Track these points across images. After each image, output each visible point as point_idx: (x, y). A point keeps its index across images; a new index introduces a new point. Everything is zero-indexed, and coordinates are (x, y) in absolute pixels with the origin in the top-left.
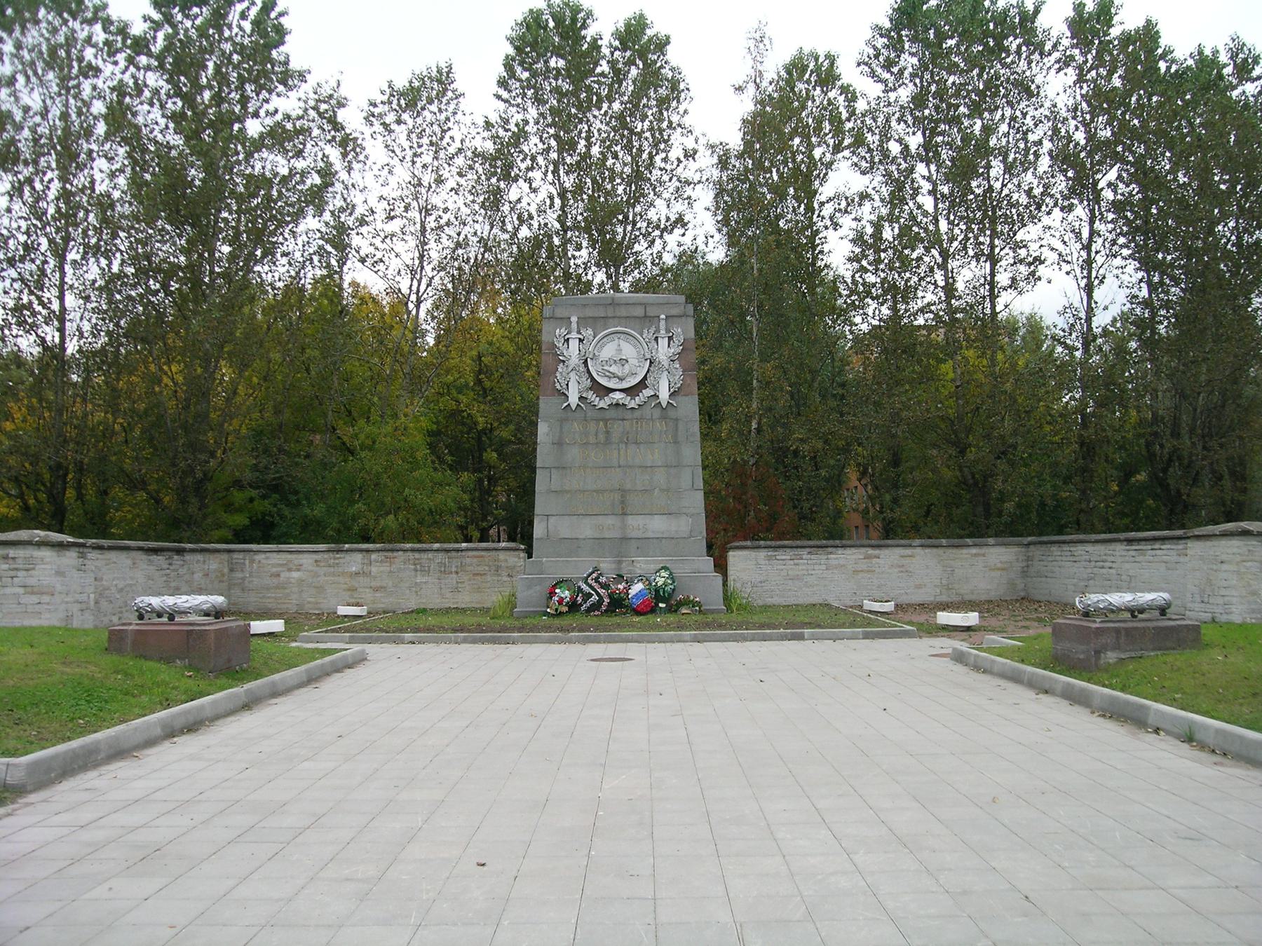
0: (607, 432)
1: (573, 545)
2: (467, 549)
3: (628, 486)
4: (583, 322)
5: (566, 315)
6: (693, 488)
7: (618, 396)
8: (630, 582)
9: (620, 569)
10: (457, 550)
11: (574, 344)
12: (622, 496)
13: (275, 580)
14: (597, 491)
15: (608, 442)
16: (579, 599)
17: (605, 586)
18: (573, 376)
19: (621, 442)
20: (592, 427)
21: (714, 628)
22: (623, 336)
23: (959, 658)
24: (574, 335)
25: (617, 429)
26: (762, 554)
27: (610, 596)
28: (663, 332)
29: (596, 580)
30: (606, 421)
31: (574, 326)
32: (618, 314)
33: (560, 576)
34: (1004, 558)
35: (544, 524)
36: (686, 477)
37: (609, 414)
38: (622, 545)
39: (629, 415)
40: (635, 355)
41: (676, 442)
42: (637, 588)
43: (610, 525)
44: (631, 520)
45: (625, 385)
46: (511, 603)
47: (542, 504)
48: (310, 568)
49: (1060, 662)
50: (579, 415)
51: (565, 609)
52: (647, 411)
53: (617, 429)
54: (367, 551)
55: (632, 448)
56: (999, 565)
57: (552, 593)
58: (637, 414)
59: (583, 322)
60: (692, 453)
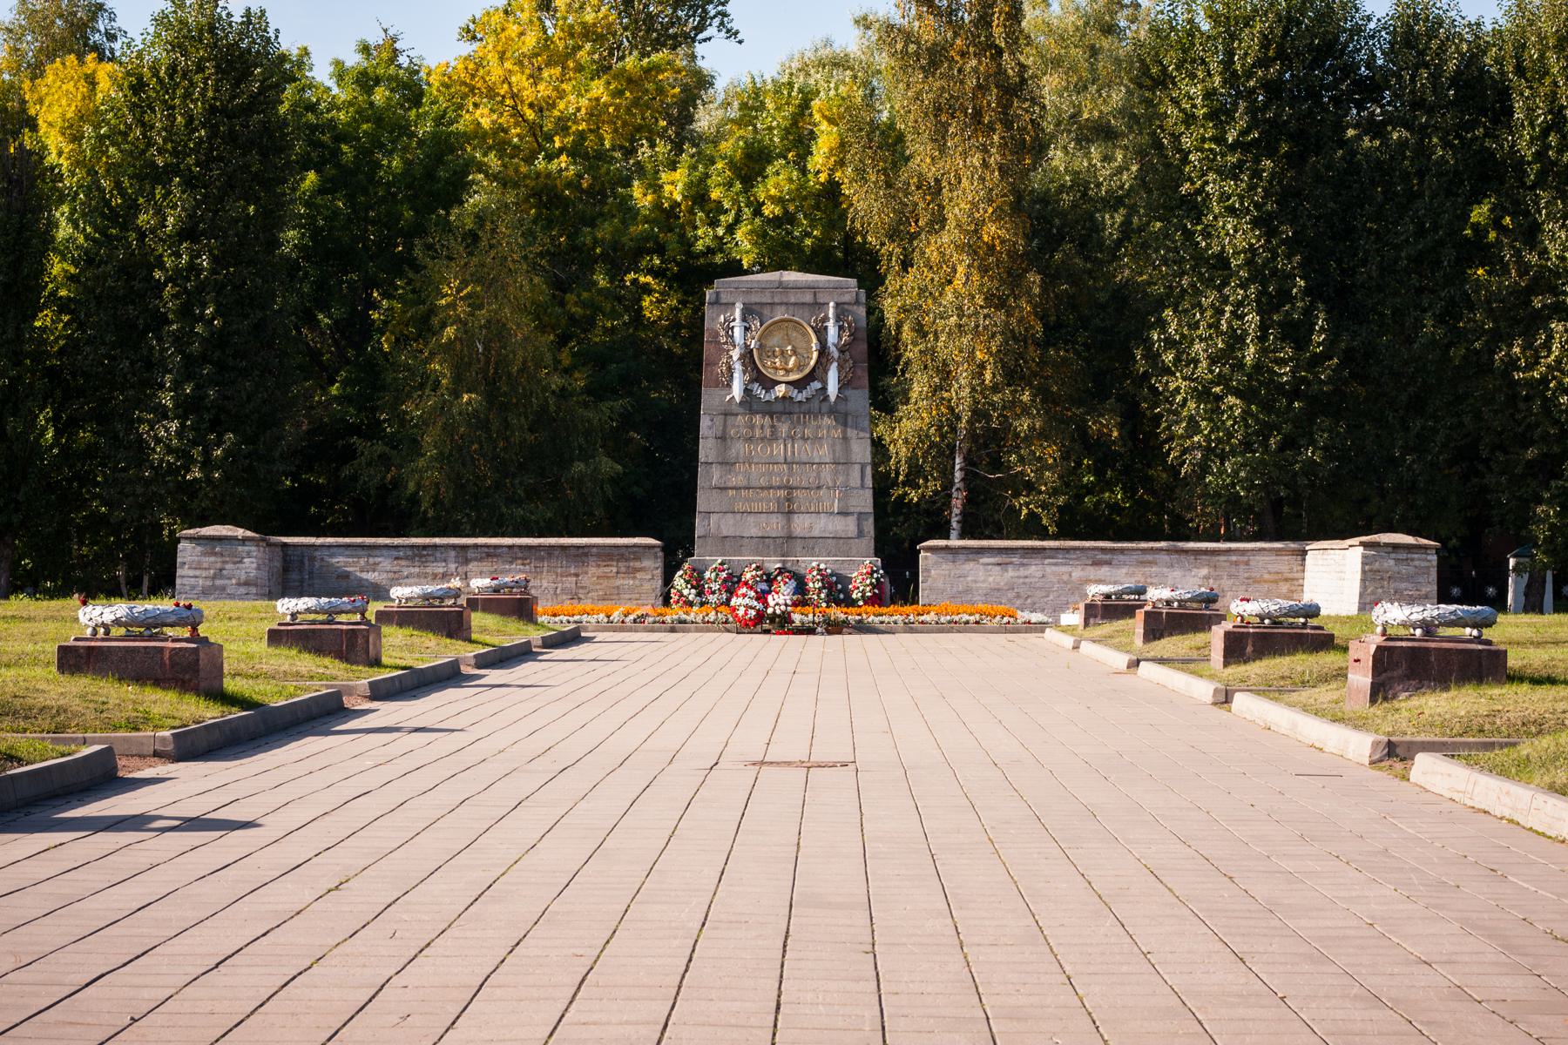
43: (775, 525)
52: (815, 404)
58: (804, 408)
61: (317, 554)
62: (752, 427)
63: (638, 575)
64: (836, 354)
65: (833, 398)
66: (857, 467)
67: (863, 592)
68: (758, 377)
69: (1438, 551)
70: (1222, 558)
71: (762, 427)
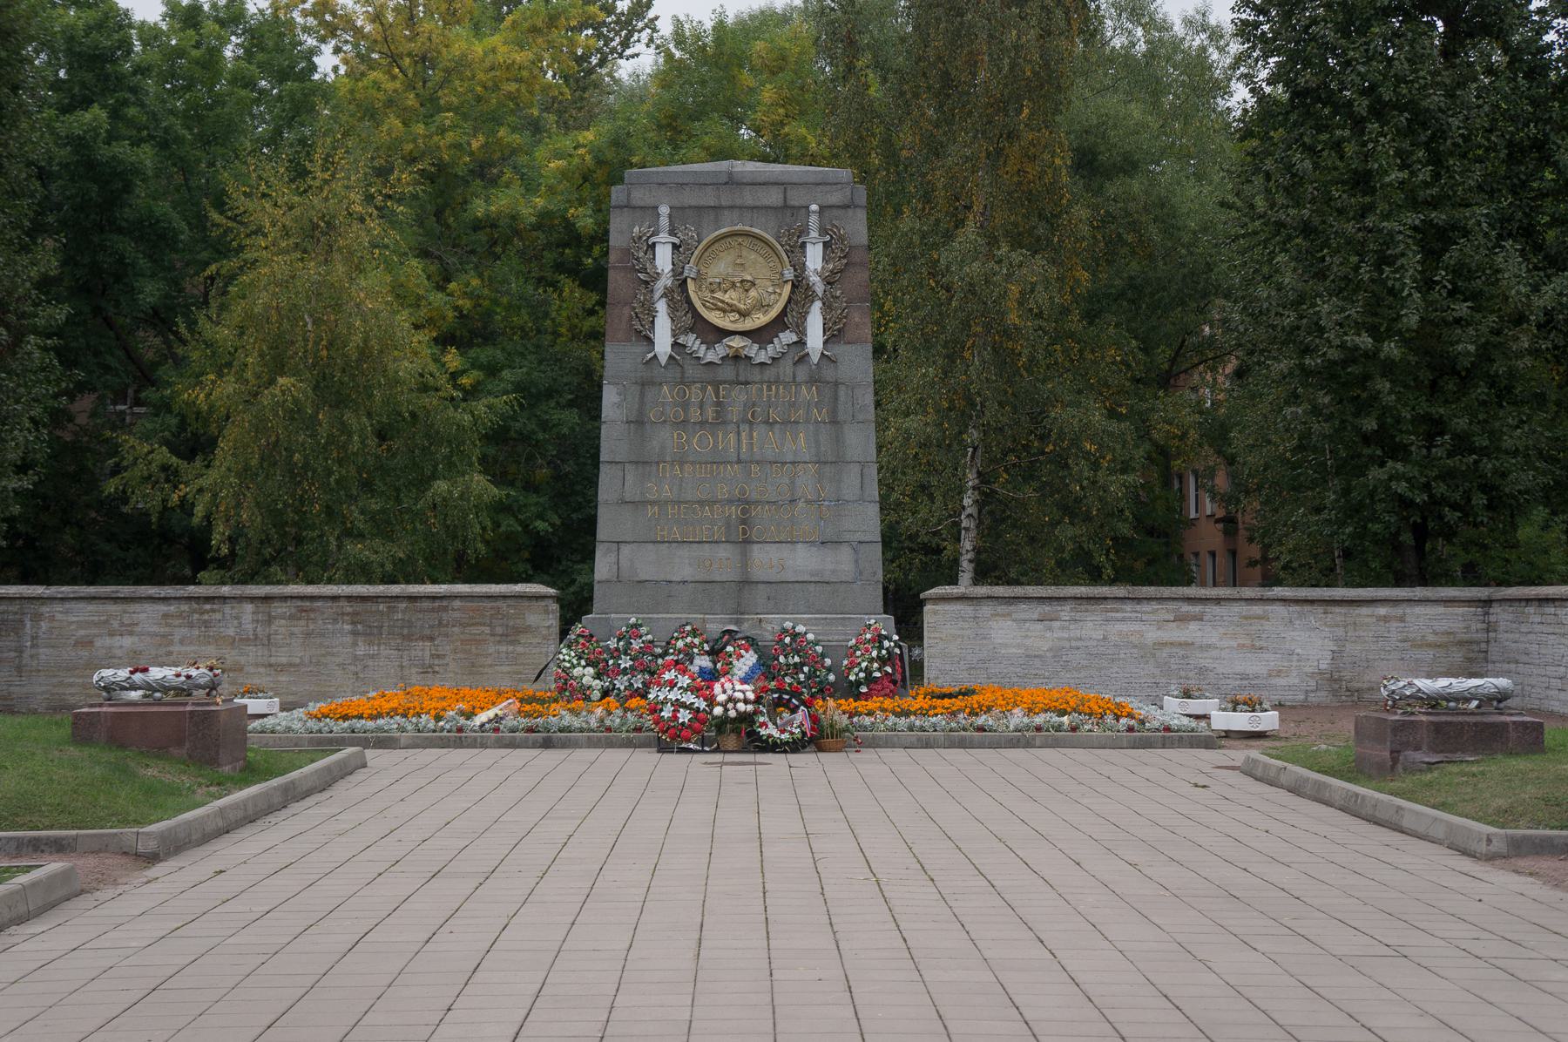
1: (660, 592)
5: (649, 201)
6: (861, 499)
12: (744, 512)
13: (85, 653)
14: (701, 503)
22: (746, 241)
23: (1249, 771)
24: (663, 237)
25: (737, 399)
30: (716, 384)
32: (738, 202)
34: (1458, 626)
35: (612, 558)
36: (851, 482)
39: (756, 375)
43: (722, 561)
45: (748, 324)
48: (155, 629)
49: (1356, 770)
52: (786, 368)
54: (267, 599)
56: (1431, 638)
58: (770, 374)
60: (861, 442)
61: (45, 609)
62: (685, 405)
63: (523, 639)
64: (819, 288)
65: (815, 358)
66: (856, 469)
67: (868, 671)
68: (692, 322)
69: (558, 599)
70: (1365, 610)
71: (701, 405)
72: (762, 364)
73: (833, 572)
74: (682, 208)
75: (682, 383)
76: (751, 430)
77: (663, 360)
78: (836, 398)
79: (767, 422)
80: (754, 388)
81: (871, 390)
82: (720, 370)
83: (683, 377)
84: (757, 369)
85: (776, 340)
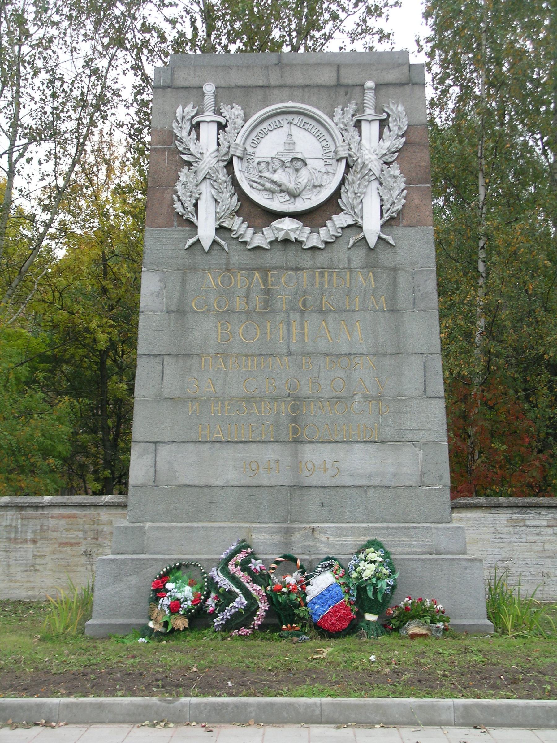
0: (268, 292)
1: (200, 499)
2: (52, 506)
3: (306, 391)
4: (225, 94)
5: (194, 82)
6: (425, 394)
7: (287, 226)
8: (308, 573)
9: (288, 544)
10: (36, 507)
11: (208, 132)
12: (295, 408)
14: (247, 399)
15: (268, 308)
16: (211, 603)
17: (261, 578)
18: (206, 190)
19: (293, 309)
20: (240, 280)
21: (495, 689)
22: (297, 119)
24: (209, 116)
25: (286, 286)
26: (503, 517)
27: (269, 598)
28: (370, 111)
29: (244, 566)
30: (265, 271)
31: (209, 100)
32: (289, 81)
33: (175, 557)
35: (148, 459)
37: (270, 259)
38: (292, 499)
39: (306, 260)
40: (320, 153)
41: (393, 311)
42: (323, 582)
43: (271, 463)
44: (312, 454)
45: (301, 205)
46: (86, 604)
47: (144, 423)
50: (216, 259)
51: (181, 623)
52: (340, 254)
53: (286, 286)
55: (313, 319)
57: (159, 591)
58: (322, 259)
59: (225, 94)
60: (424, 331)
66: (416, 363)
72: (314, 248)
73: (395, 475)
74: (229, 88)
75: (228, 270)
76: (302, 319)
77: (206, 245)
78: (395, 284)
79: (320, 311)
80: (304, 276)
81: (434, 276)
82: (268, 256)
83: (228, 264)
84: (309, 254)
85: (329, 223)
